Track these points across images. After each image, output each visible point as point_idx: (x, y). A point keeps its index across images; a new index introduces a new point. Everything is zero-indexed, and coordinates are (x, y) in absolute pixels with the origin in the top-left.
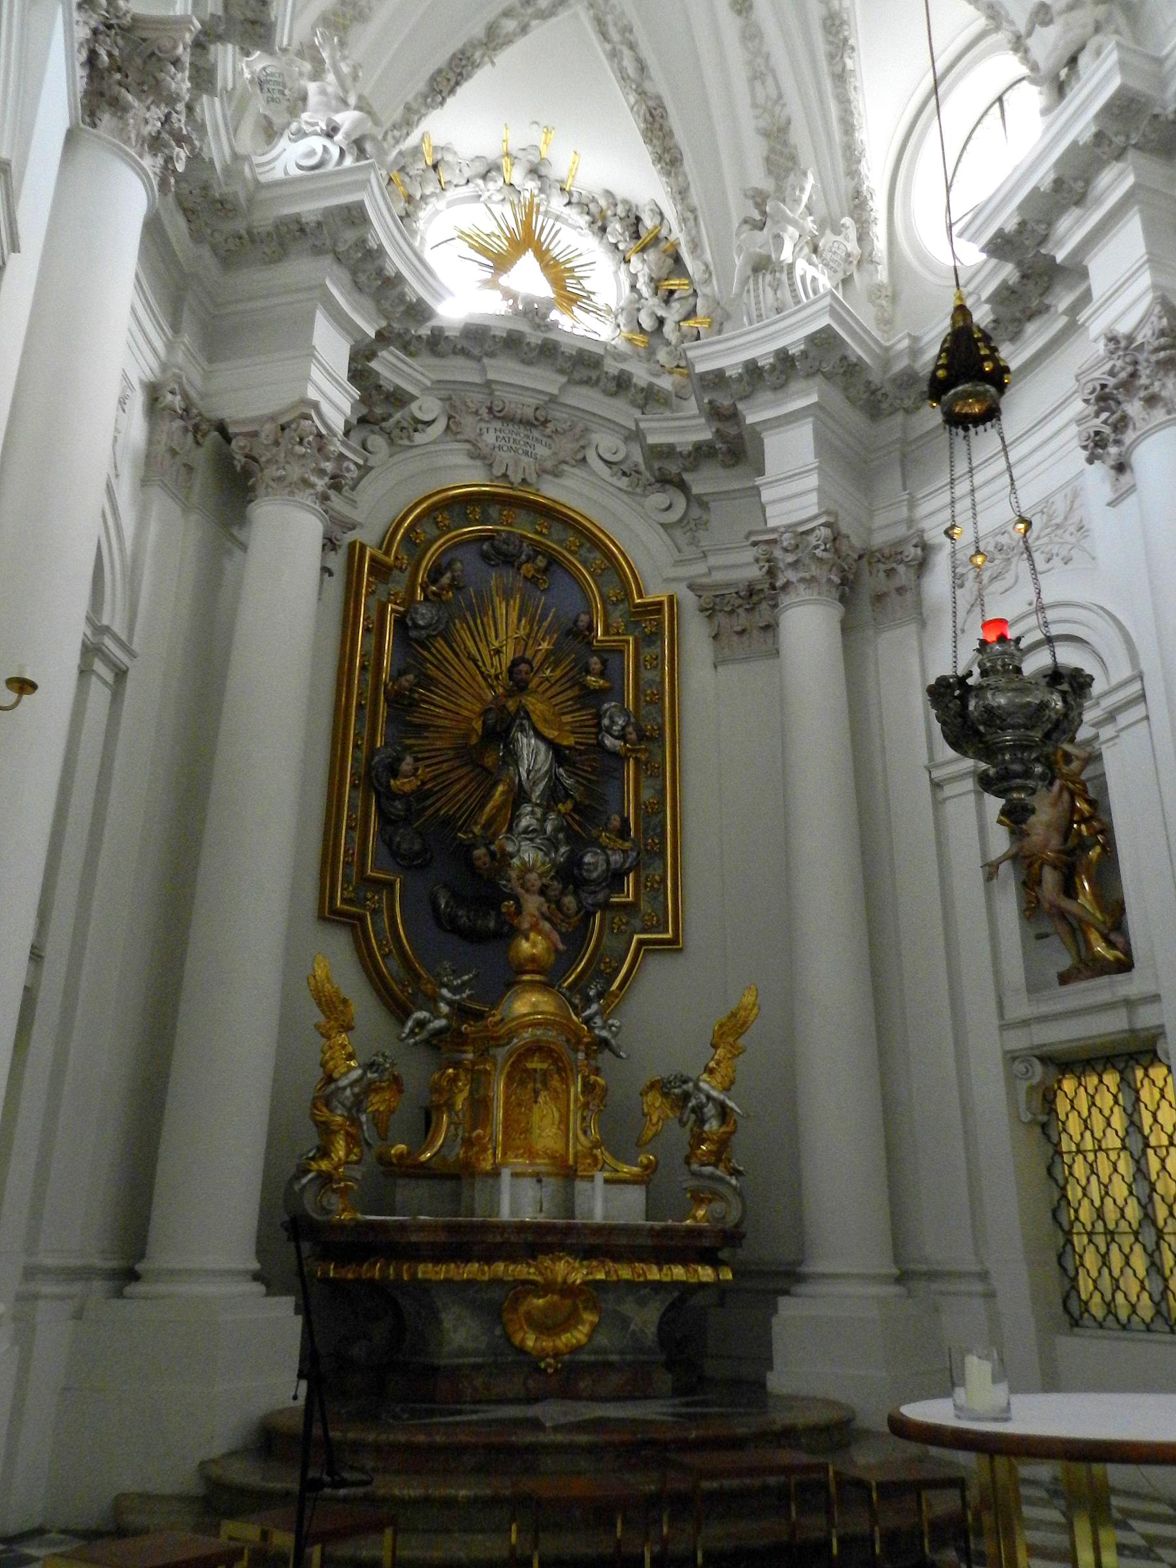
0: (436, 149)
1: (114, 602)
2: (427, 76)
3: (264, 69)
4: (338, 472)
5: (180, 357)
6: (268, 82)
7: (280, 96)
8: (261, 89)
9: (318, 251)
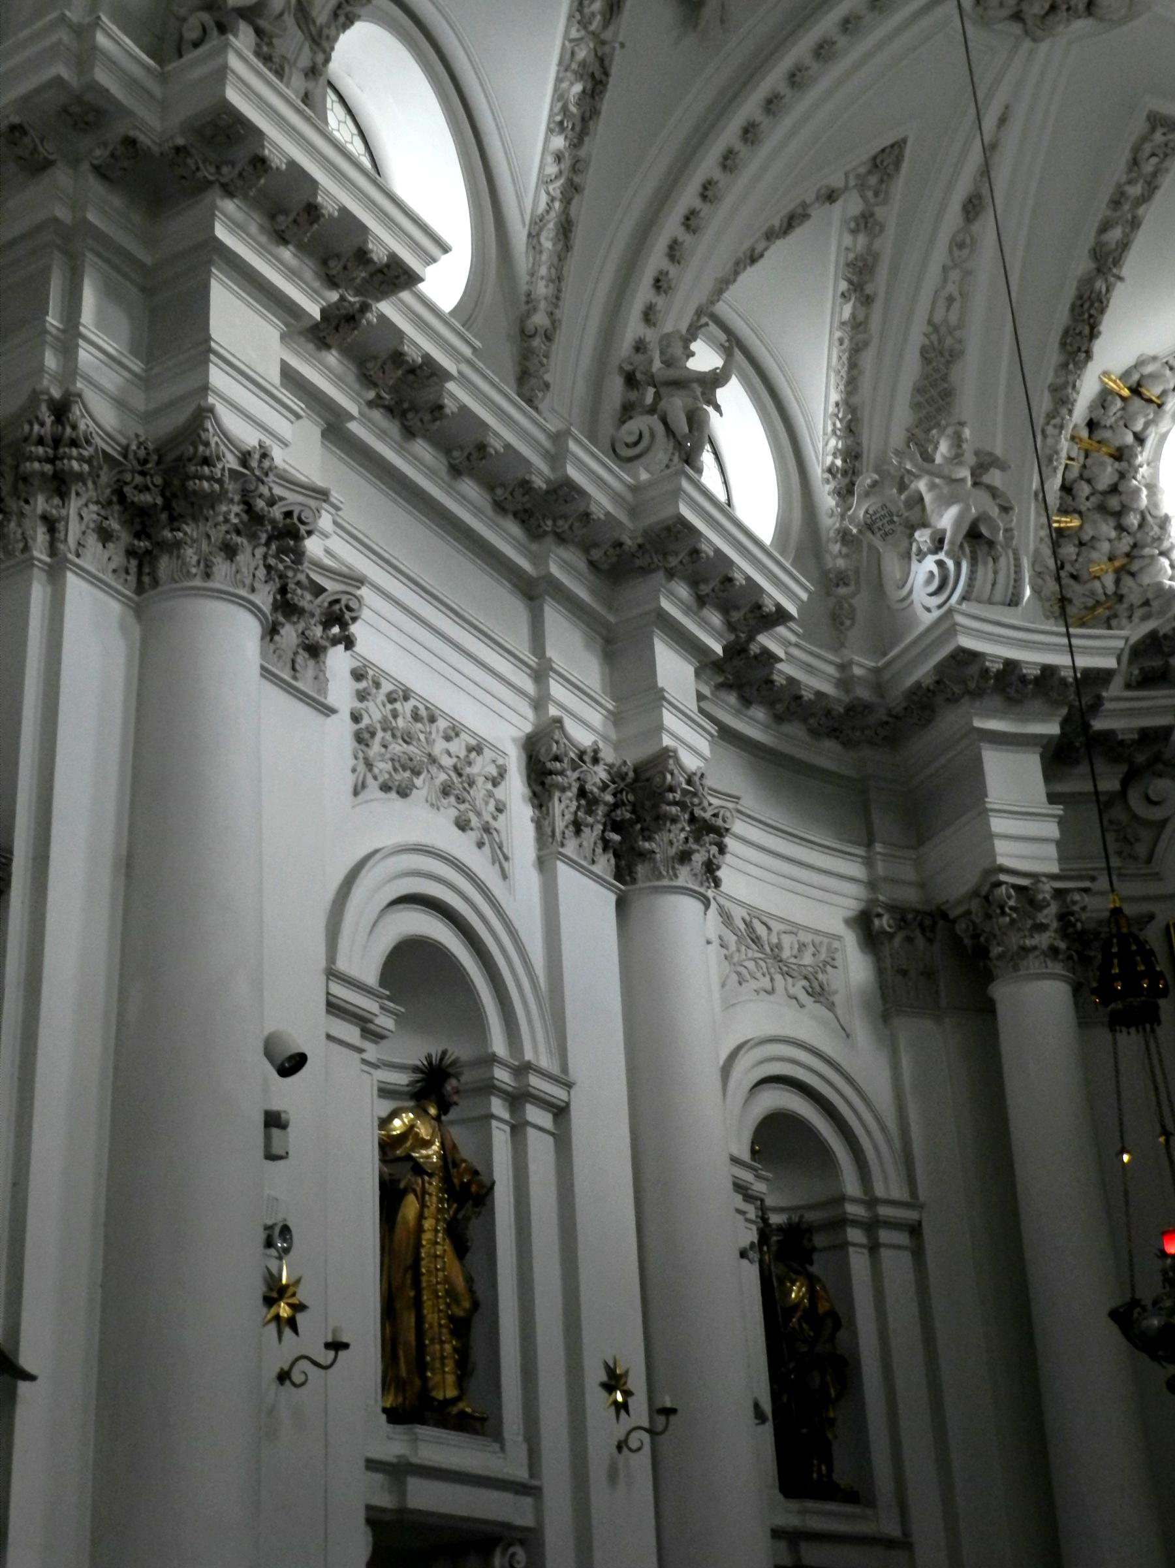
0: (1125, 376)
1: (881, 1164)
2: (1056, 346)
3: (867, 512)
4: (1065, 910)
5: (880, 869)
6: (874, 522)
7: (892, 526)
8: (873, 533)
9: (953, 700)
